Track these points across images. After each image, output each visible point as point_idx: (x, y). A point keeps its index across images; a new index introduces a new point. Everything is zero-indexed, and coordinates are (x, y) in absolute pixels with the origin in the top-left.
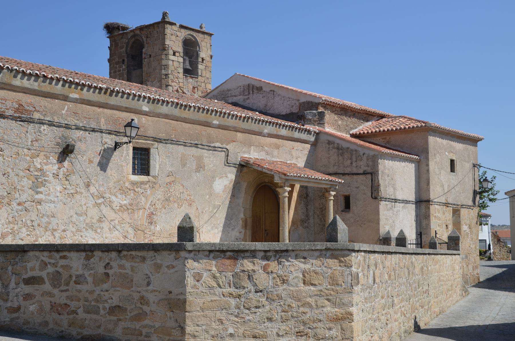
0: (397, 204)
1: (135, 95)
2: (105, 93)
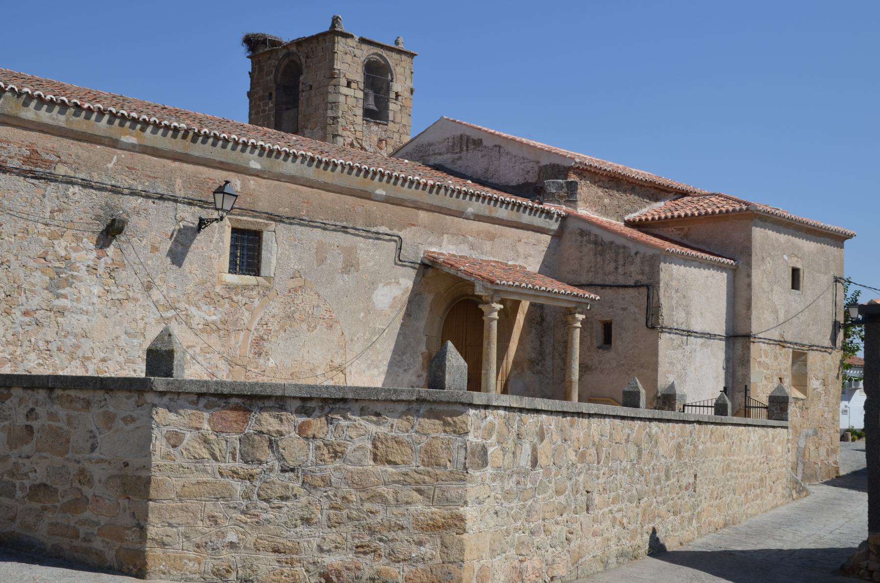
1: (236, 143)
2: (184, 137)
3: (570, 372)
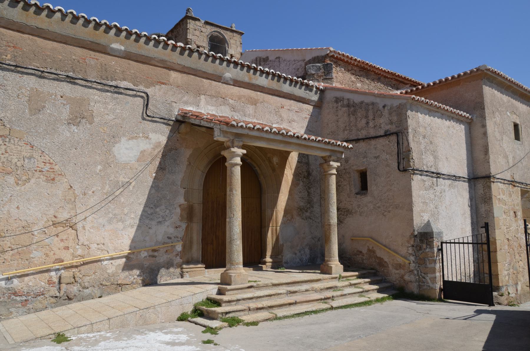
0: (440, 180)
3: (329, 216)
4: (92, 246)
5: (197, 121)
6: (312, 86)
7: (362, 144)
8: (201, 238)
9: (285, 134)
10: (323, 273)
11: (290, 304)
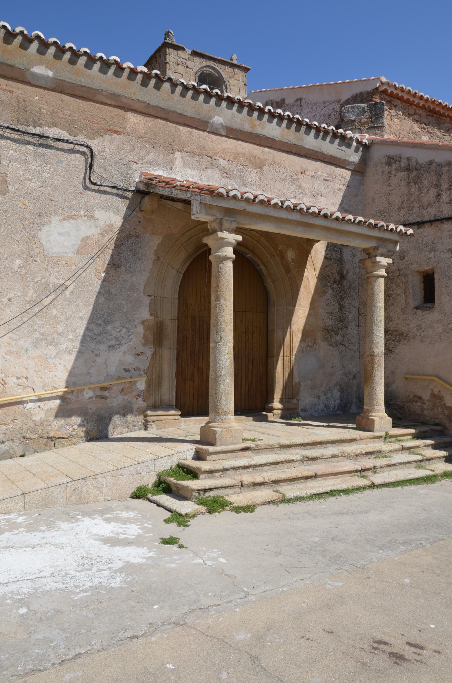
3: (372, 341)
4: (8, 380)
5: (167, 190)
6: (351, 138)
7: (428, 230)
8: (174, 371)
9: (305, 210)
10: (359, 428)
11: (307, 478)
